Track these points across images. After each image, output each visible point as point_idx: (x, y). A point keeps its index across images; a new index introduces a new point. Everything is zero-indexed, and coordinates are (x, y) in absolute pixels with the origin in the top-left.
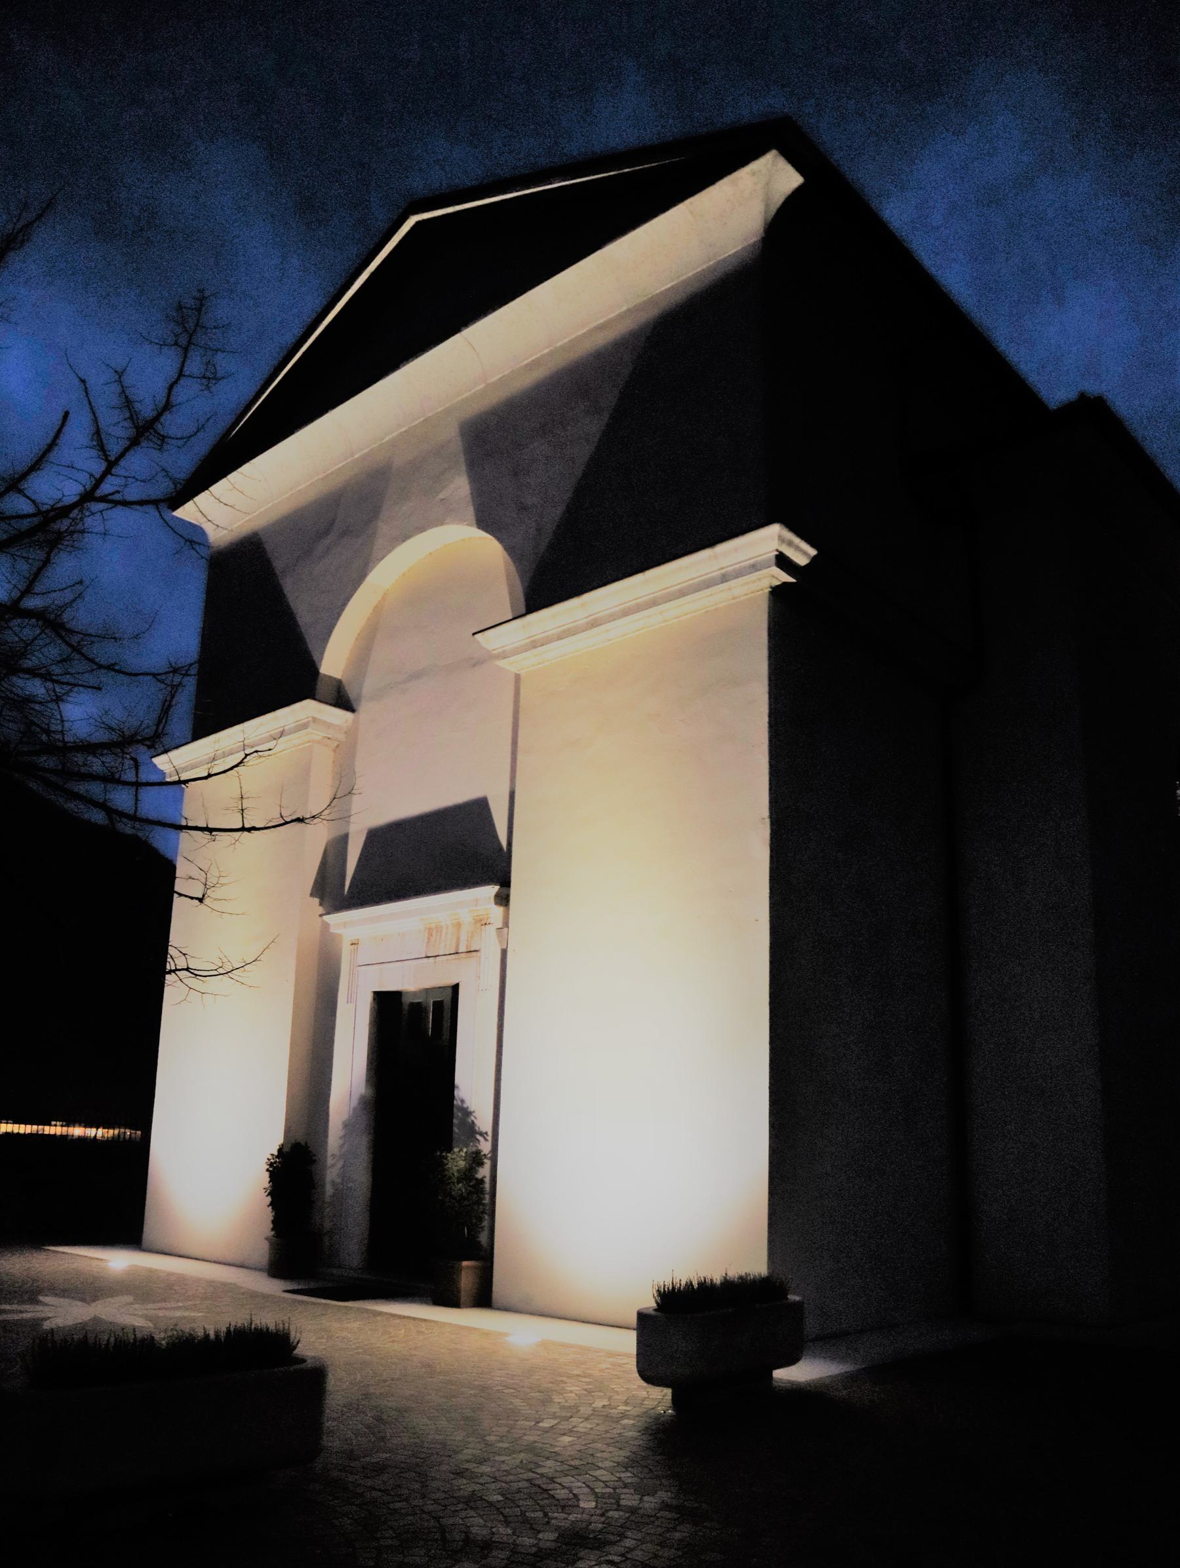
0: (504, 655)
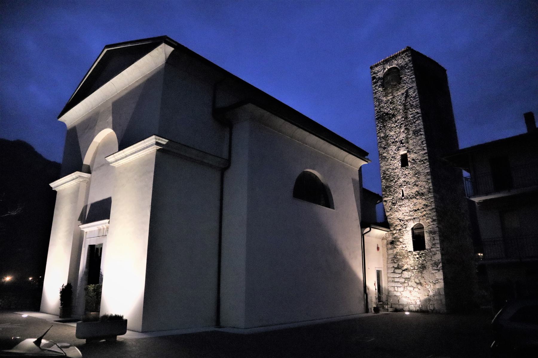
0: (111, 163)
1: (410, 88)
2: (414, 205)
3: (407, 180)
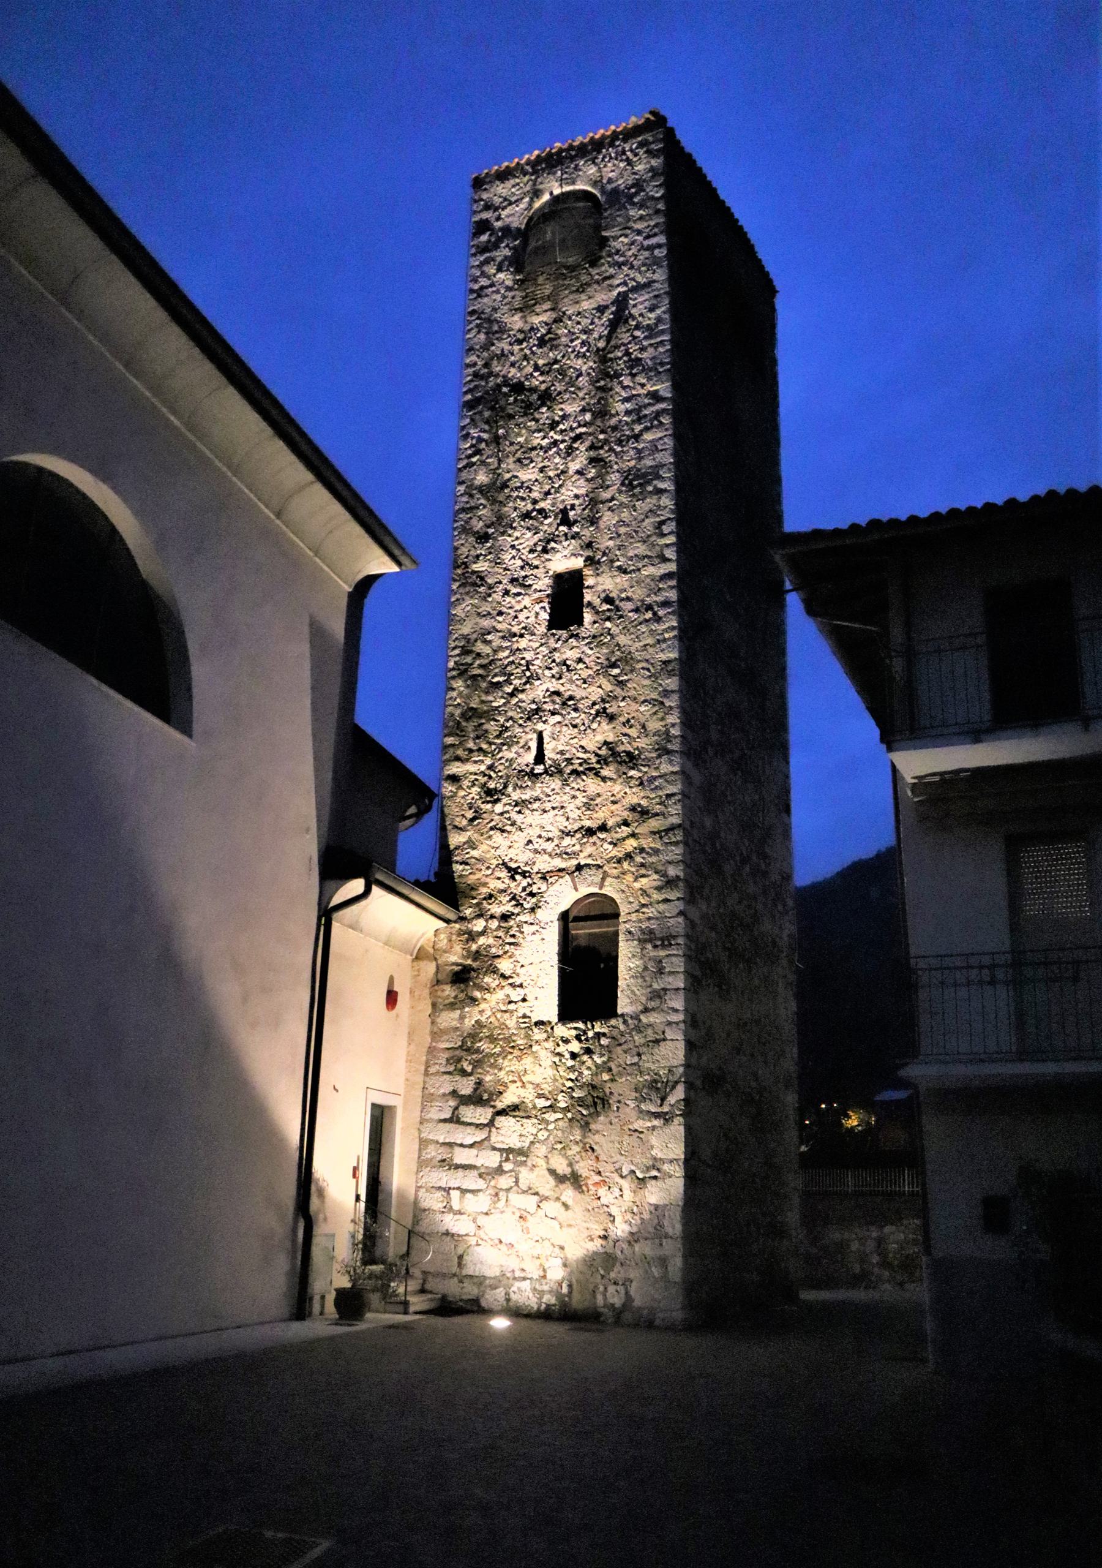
1: (638, 288)
2: (588, 806)
3: (567, 689)
